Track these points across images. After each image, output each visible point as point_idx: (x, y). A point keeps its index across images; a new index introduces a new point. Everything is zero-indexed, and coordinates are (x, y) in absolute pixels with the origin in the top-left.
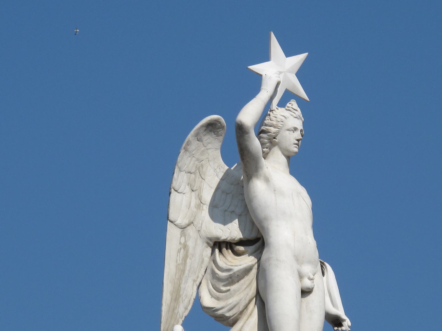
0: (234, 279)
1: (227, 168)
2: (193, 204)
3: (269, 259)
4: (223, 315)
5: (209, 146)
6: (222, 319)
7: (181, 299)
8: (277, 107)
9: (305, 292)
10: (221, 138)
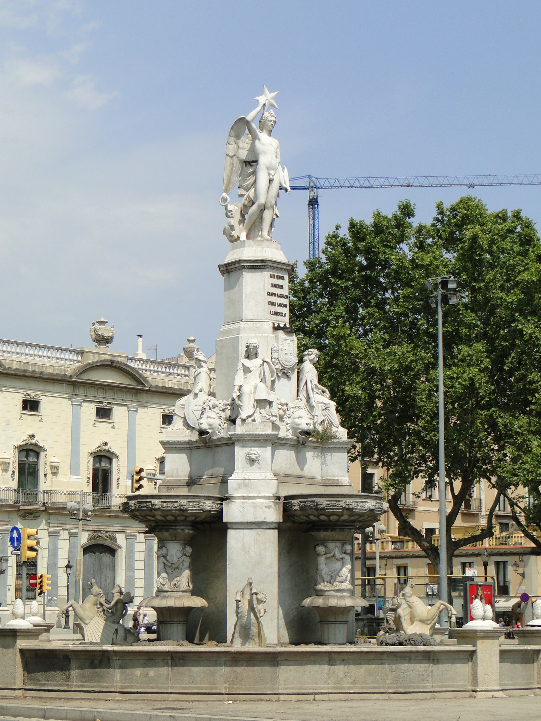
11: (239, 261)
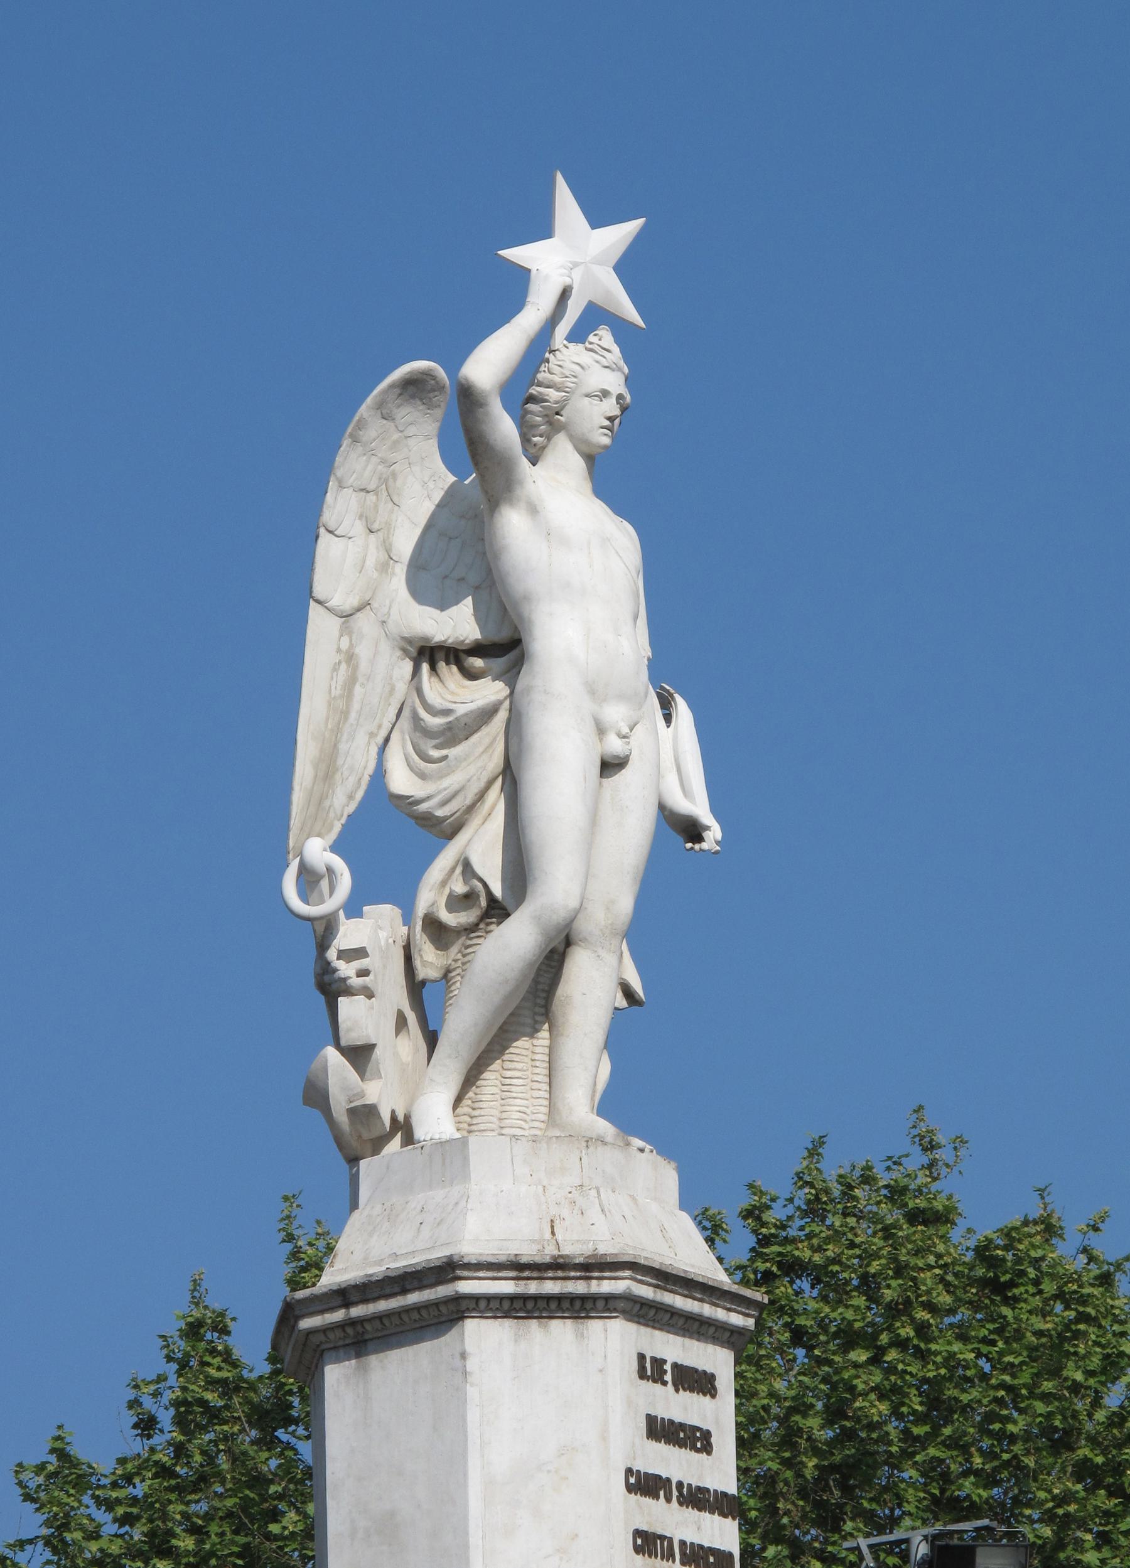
0: (457, 732)
1: (452, 479)
2: (371, 562)
3: (529, 689)
4: (430, 813)
5: (411, 430)
6: (428, 821)
7: (338, 776)
8: (565, 342)
9: (610, 766)
10: (439, 413)
11: (448, 1269)
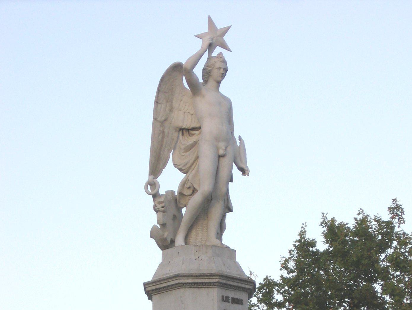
2: (167, 109)
